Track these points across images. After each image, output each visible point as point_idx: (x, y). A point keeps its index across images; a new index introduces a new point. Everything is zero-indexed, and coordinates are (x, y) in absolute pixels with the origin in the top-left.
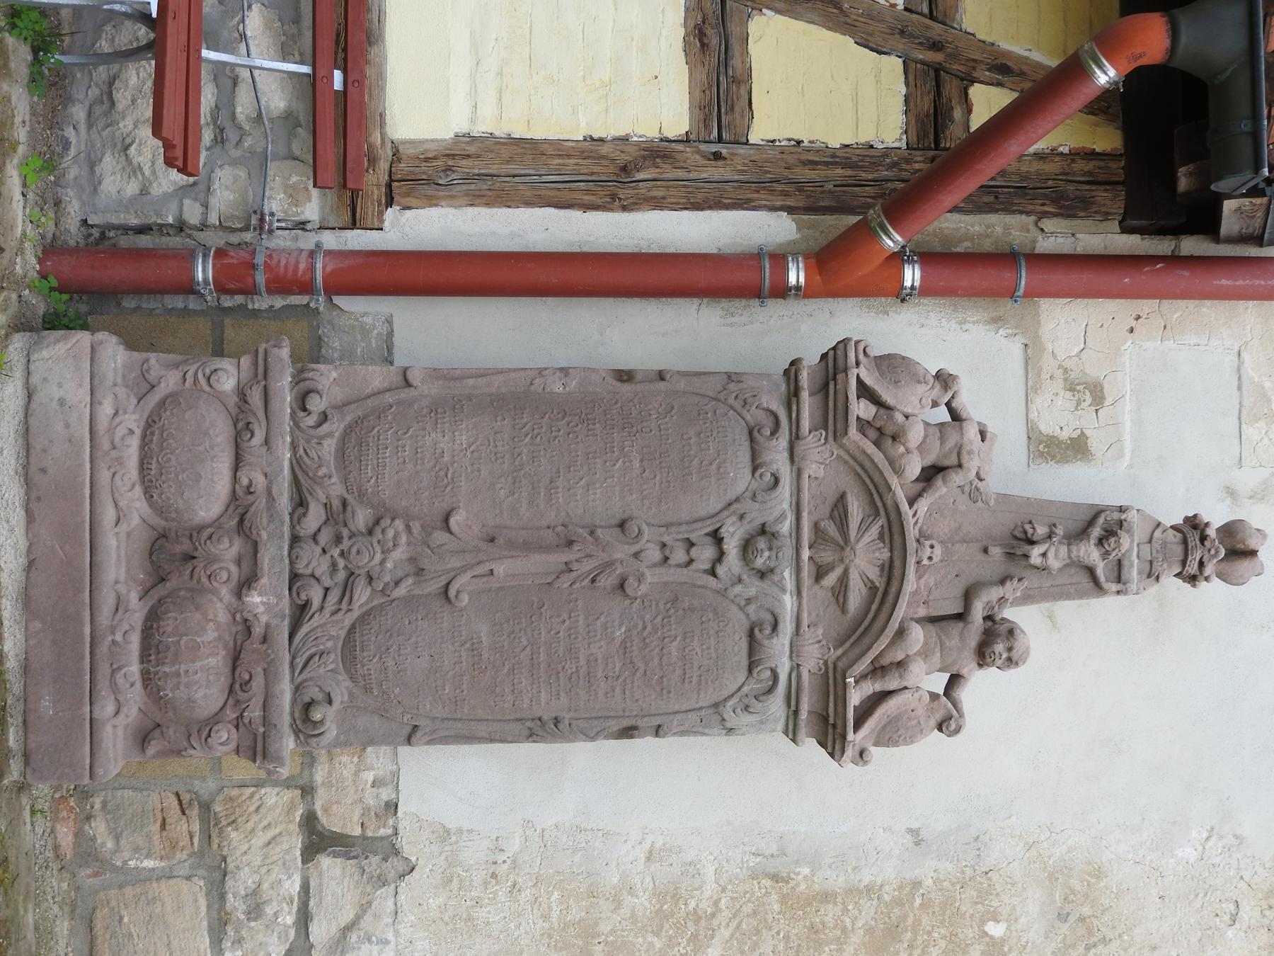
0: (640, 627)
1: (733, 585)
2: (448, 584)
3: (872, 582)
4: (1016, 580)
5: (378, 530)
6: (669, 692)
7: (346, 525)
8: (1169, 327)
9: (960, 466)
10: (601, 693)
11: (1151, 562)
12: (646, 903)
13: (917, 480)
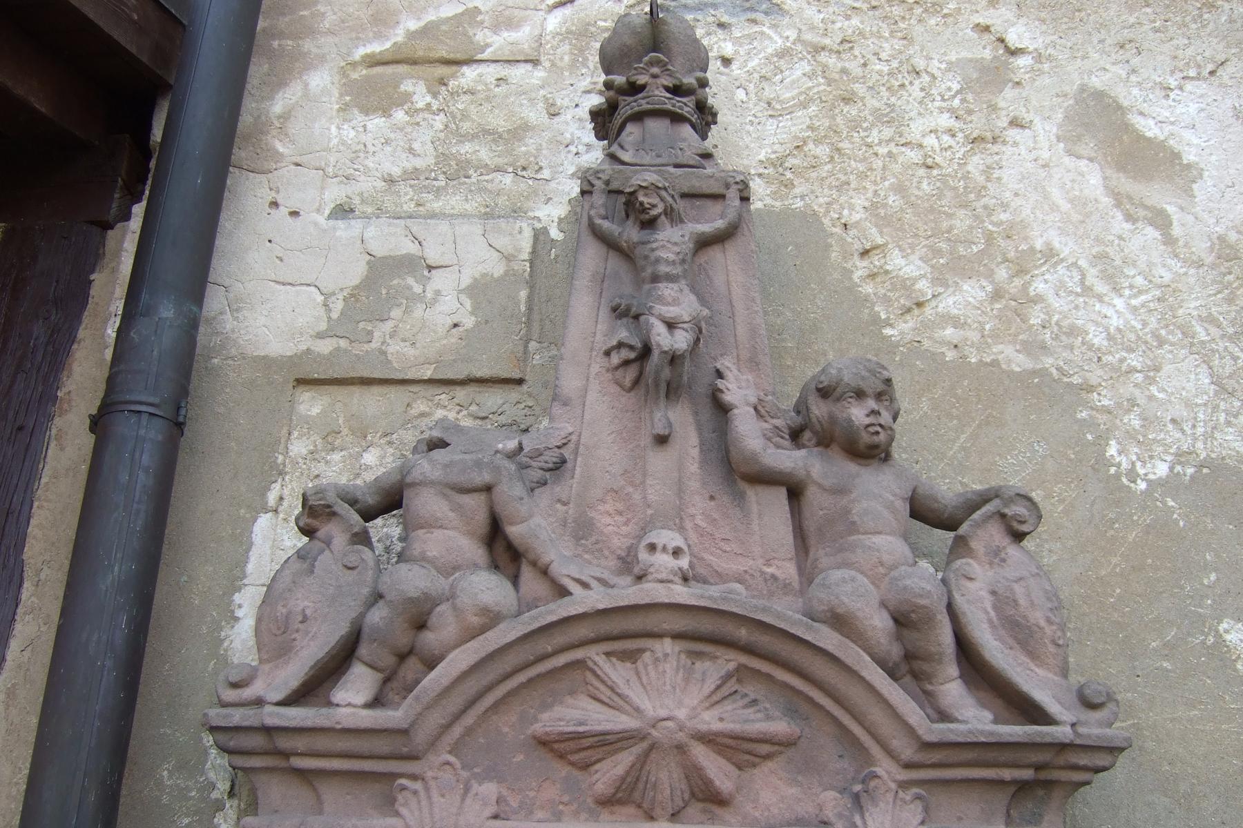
4: (720, 384)
8: (298, 159)
9: (488, 489)
13: (515, 580)
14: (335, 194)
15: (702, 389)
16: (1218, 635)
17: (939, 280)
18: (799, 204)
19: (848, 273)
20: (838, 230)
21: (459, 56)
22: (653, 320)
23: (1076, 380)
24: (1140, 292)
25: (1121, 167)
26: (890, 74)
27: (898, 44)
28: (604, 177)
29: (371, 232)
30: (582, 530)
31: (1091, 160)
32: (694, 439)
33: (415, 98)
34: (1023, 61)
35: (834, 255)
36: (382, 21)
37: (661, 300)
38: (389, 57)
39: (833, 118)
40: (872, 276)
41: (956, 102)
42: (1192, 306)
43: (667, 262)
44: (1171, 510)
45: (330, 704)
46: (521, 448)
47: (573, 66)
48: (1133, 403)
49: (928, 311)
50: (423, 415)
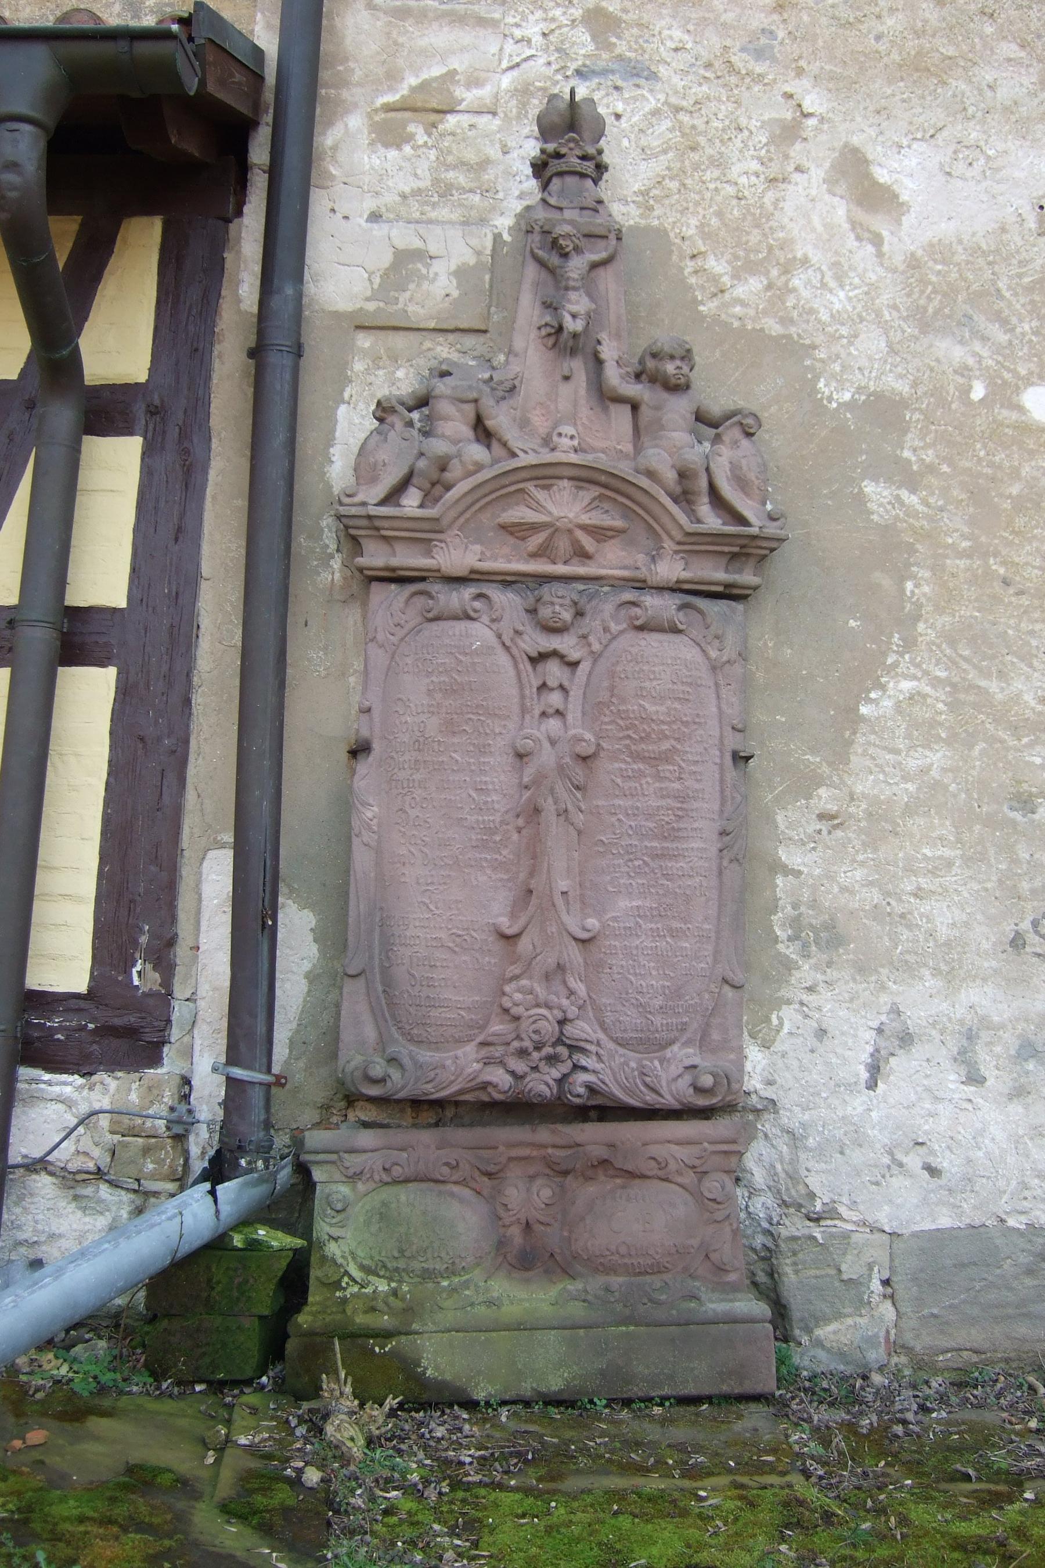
0: (628, 742)
1: (590, 645)
2: (575, 939)
3: (594, 499)
4: (599, 348)
5: (515, 1011)
6: (698, 715)
7: (508, 1044)
9: (476, 401)
10: (697, 786)
11: (582, 209)
12: (939, 755)
13: (489, 447)
14: (370, 204)
15: (589, 350)
16: (861, 488)
17: (736, 276)
18: (656, 222)
19: (681, 269)
20: (678, 241)
21: (445, 108)
22: (565, 313)
23: (807, 342)
24: (856, 288)
25: (860, 203)
26: (723, 130)
27: (731, 106)
28: (540, 223)
29: (394, 233)
30: (524, 423)
31: (842, 197)
32: (584, 378)
33: (417, 137)
34: (811, 122)
35: (675, 258)
36: (393, 77)
37: (569, 301)
38: (399, 106)
39: (683, 162)
40: (696, 272)
41: (764, 151)
42: (885, 298)
43: (574, 280)
44: (848, 420)
45: (400, 506)
46: (491, 378)
47: (518, 117)
48: (838, 356)
49: (727, 296)
50: (429, 349)
